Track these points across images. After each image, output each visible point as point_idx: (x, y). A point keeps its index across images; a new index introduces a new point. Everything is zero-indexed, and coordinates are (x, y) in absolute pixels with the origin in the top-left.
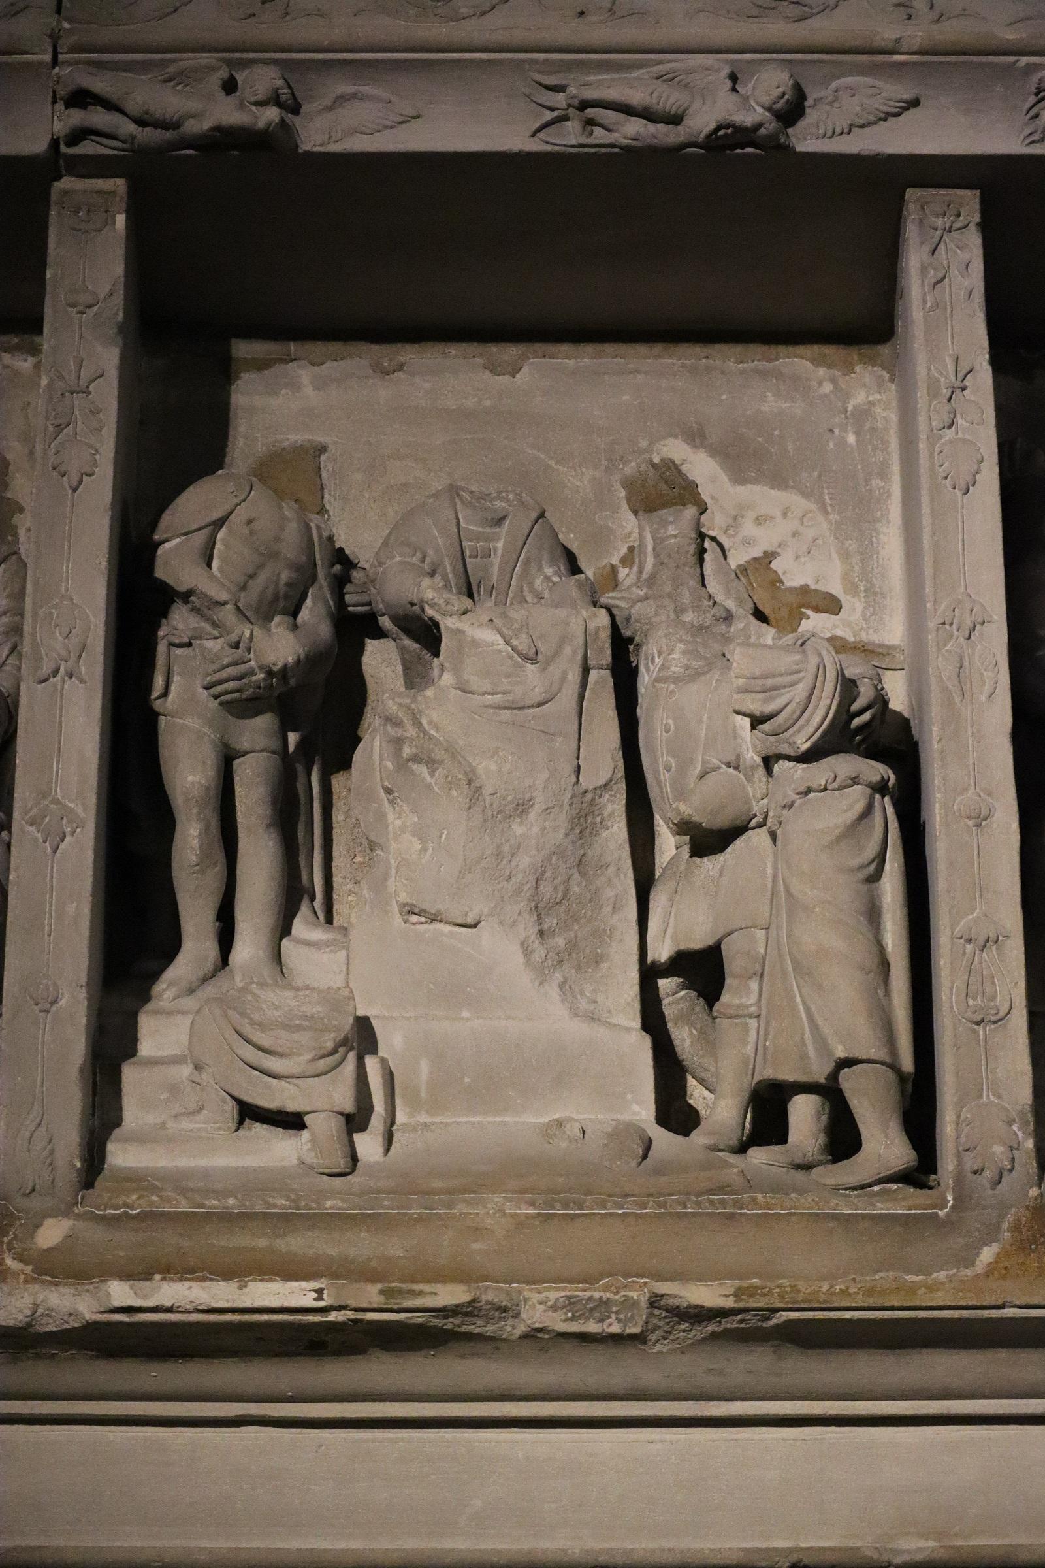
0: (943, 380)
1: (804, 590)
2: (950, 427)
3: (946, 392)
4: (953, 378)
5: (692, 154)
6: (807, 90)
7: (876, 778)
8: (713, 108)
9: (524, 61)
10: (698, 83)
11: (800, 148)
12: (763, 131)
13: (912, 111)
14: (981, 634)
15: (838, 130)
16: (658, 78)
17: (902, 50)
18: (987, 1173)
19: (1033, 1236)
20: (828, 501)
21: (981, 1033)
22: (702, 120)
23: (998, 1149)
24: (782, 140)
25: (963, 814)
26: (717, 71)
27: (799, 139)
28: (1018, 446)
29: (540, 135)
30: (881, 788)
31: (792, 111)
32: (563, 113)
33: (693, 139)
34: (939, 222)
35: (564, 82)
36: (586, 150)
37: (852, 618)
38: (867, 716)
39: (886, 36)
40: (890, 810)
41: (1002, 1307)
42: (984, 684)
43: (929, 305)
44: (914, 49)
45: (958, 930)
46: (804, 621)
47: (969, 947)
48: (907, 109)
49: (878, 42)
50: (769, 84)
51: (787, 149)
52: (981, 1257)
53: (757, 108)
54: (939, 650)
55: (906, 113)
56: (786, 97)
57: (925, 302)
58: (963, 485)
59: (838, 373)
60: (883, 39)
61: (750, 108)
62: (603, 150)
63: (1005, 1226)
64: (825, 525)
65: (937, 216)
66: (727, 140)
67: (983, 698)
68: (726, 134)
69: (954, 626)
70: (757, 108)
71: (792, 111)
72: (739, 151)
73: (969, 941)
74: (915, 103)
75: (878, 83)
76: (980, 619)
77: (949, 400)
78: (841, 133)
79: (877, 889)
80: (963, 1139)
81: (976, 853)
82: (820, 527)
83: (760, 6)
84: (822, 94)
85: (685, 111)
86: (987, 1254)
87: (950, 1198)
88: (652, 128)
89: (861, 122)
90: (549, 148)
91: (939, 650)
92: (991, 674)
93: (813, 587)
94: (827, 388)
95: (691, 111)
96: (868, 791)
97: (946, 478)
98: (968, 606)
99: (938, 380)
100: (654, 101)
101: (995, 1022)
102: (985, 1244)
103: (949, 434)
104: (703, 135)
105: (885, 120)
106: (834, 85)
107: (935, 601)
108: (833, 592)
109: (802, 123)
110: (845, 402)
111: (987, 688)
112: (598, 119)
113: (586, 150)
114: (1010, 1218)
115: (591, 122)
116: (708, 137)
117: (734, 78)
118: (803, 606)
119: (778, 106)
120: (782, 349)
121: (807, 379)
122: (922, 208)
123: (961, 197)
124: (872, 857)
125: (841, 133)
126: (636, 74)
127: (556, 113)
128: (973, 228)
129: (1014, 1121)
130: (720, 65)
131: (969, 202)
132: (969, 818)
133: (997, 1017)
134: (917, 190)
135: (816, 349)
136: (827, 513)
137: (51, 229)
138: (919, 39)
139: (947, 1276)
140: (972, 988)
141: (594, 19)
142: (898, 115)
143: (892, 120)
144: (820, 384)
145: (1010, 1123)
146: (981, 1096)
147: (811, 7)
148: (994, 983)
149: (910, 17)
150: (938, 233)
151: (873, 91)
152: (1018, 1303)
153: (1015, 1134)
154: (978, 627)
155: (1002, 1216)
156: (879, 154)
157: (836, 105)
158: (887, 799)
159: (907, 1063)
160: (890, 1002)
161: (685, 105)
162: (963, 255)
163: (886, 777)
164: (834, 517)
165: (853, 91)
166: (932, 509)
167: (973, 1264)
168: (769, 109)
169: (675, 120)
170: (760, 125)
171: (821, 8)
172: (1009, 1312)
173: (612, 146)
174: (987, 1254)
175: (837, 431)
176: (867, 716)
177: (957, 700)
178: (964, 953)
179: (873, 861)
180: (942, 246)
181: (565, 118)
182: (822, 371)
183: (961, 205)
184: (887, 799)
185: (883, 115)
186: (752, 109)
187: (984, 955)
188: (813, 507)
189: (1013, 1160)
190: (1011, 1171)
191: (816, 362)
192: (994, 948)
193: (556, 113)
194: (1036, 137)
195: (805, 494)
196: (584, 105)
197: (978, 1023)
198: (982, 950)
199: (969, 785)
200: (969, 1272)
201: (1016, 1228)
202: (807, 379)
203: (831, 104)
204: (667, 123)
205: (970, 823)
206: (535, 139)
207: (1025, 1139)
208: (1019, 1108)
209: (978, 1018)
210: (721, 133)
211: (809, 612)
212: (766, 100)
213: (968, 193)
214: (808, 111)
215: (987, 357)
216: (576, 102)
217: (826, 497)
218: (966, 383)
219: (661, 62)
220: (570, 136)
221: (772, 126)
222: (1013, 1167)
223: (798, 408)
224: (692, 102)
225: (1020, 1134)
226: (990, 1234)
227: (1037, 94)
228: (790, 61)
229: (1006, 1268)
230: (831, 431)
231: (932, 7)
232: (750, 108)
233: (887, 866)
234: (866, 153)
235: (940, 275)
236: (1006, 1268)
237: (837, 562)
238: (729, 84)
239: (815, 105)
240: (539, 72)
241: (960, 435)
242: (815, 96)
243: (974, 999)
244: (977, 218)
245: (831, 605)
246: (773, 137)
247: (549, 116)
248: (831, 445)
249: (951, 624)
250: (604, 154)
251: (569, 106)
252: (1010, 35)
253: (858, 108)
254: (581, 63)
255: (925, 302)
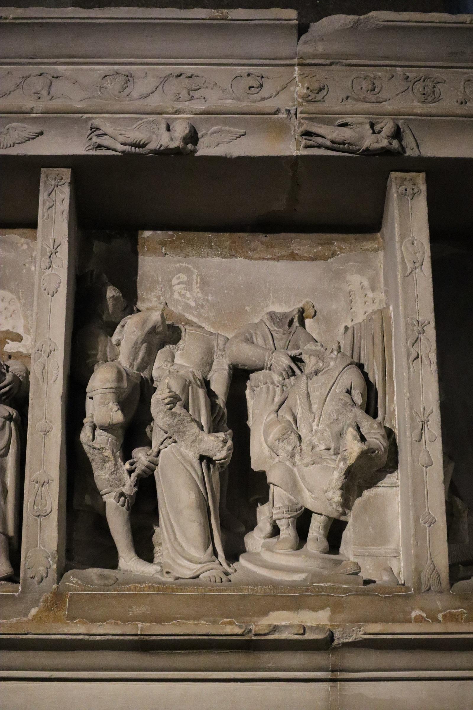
0: (48, 249)
1: (8, 332)
2: (49, 269)
3: (49, 254)
4: (52, 248)
7: (7, 414)
13: (40, 137)
14: (53, 355)
15: (9, 145)
18: (36, 578)
19: (53, 605)
20: (21, 295)
21: (39, 520)
23: (41, 568)
25: (39, 430)
28: (95, 273)
30: (10, 418)
34: (53, 182)
37: (26, 344)
38: (7, 388)
39: (27, 107)
40: (13, 427)
41: (27, 634)
42: (52, 376)
43: (45, 217)
45: (32, 478)
46: (6, 345)
47: (37, 485)
48: (38, 136)
49: (24, 109)
52: (31, 613)
54: (35, 361)
57: (43, 216)
58: (51, 292)
59: (30, 241)
63: (42, 600)
64: (19, 305)
65: (52, 180)
67: (52, 382)
69: (43, 352)
73: (37, 482)
74: (41, 133)
75: (26, 126)
76: (53, 349)
77: (50, 257)
78: (10, 146)
79: (5, 460)
80: (27, 564)
81: (43, 446)
82: (17, 305)
86: (34, 611)
87: (20, 588)
89: (18, 142)
91: (35, 361)
92: (56, 372)
93: (11, 330)
94: (25, 247)
96: (3, 420)
97: (45, 290)
98: (49, 343)
99: (46, 249)
101: (45, 516)
102: (33, 607)
103: (48, 271)
105: (29, 140)
106: (7, 127)
107: (35, 342)
108: (20, 333)
110: (32, 253)
111: (54, 378)
114: (44, 597)
118: (6, 338)
120: (8, 231)
121: (17, 243)
122: (47, 176)
123: (63, 171)
124: (2, 447)
125: (10, 146)
128: (67, 184)
129: (49, 557)
131: (66, 173)
132: (41, 431)
133: (46, 514)
135: (21, 231)
136: (20, 299)
137: (353, 16)
139: (16, 620)
140: (37, 502)
142: (34, 139)
144: (22, 245)
145: (47, 558)
146: (37, 546)
148: (46, 500)
149: (39, 98)
150: (53, 186)
151: (23, 129)
152: (33, 633)
153: (49, 562)
154: (52, 352)
155: (40, 596)
157: (8, 135)
158: (12, 423)
159: (11, 531)
160: (6, 507)
162: (62, 196)
163: (11, 414)
164: (23, 301)
165: (15, 129)
166: (38, 303)
167: (27, 615)
172: (30, 636)
174: (34, 611)
175: (27, 265)
176: (7, 388)
177: (41, 383)
178: (35, 488)
179: (3, 449)
180: (54, 192)
182: (23, 240)
183: (63, 175)
184: (12, 423)
185: (27, 139)
187: (43, 488)
188: (15, 297)
189: (47, 573)
190: (46, 577)
191: (21, 236)
192: (47, 485)
194: (90, 148)
195: (11, 291)
197: (38, 516)
198: (42, 486)
199: (43, 418)
200: (25, 619)
201: (46, 601)
202: (17, 243)
205: (42, 433)
207: (53, 565)
208: (52, 551)
209: (37, 514)
211: (9, 341)
213: (66, 170)
215: (67, 239)
217: (20, 293)
218: (57, 250)
222: (47, 576)
223: (12, 255)
225: (51, 562)
226: (35, 603)
227: (91, 130)
229: (40, 617)
230: (25, 265)
233: (10, 451)
235: (51, 205)
236: (40, 617)
237: (23, 321)
241: (53, 272)
243: (37, 506)
244: (69, 181)
245: (18, 338)
248: (24, 271)
249: (41, 351)
252: (79, 106)
255: (43, 216)
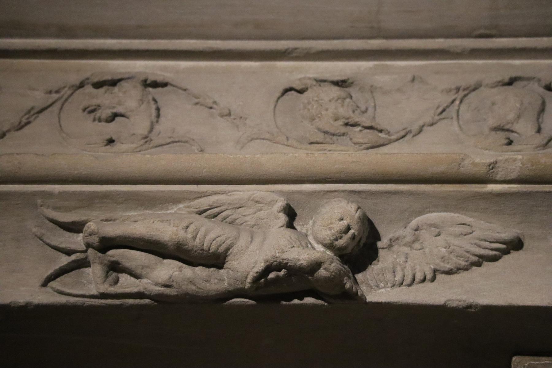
5: (240, 307)
6: (381, 229)
8: (259, 243)
9: (35, 194)
10: (247, 218)
11: (370, 298)
12: (322, 272)
13: (514, 255)
15: (419, 276)
16: (201, 213)
17: (498, 177)
22: (247, 262)
24: (348, 286)
26: (272, 203)
27: (368, 285)
29: (53, 284)
31: (361, 250)
32: (82, 256)
33: (239, 285)
35: (84, 218)
36: (109, 301)
39: (477, 160)
44: (513, 176)
48: (506, 252)
49: (467, 168)
50: (333, 217)
51: (352, 297)
53: (316, 245)
55: (506, 257)
56: (352, 232)
60: (474, 164)
61: (307, 245)
62: (131, 301)
66: (281, 284)
68: (278, 277)
70: (316, 245)
71: (361, 250)
72: (296, 301)
74: (516, 245)
75: (468, 220)
78: (424, 280)
83: (326, 133)
84: (400, 232)
85: (227, 250)
88: (188, 271)
89: (448, 267)
90: (63, 299)
95: (235, 250)
100: (189, 236)
104: (249, 280)
106: (414, 222)
109: (374, 268)
112: (126, 263)
113: (109, 301)
115: (115, 268)
116: (256, 280)
117: (291, 214)
119: (340, 243)
125: (424, 280)
126: (174, 209)
127: (73, 257)
130: (274, 196)
134: (527, 358)
138: (519, 164)
141: (124, 147)
142: (494, 259)
143: (487, 266)
147: (388, 133)
149: (510, 143)
156: (470, 306)
157: (417, 245)
161: (229, 242)
165: (438, 229)
168: (330, 246)
169: (216, 260)
170: (317, 265)
171: (402, 133)
173: (140, 295)
181: (83, 264)
185: (476, 259)
186: (310, 245)
193: (73, 257)
196: (106, 244)
203: (410, 245)
204: (209, 266)
206: (48, 289)
210: (272, 275)
212: (327, 235)
214: (381, 253)
216: (95, 240)
219: (202, 195)
220: (91, 283)
221: (332, 266)
224: (237, 238)
228: (360, 192)
231: (539, 131)
232: (307, 245)
234: (454, 305)
238: (283, 218)
239: (390, 246)
240: (56, 208)
242: (391, 236)
246: (335, 280)
247: (65, 260)
250: (132, 306)
251: (88, 245)
253: (443, 250)
254: (106, 196)
